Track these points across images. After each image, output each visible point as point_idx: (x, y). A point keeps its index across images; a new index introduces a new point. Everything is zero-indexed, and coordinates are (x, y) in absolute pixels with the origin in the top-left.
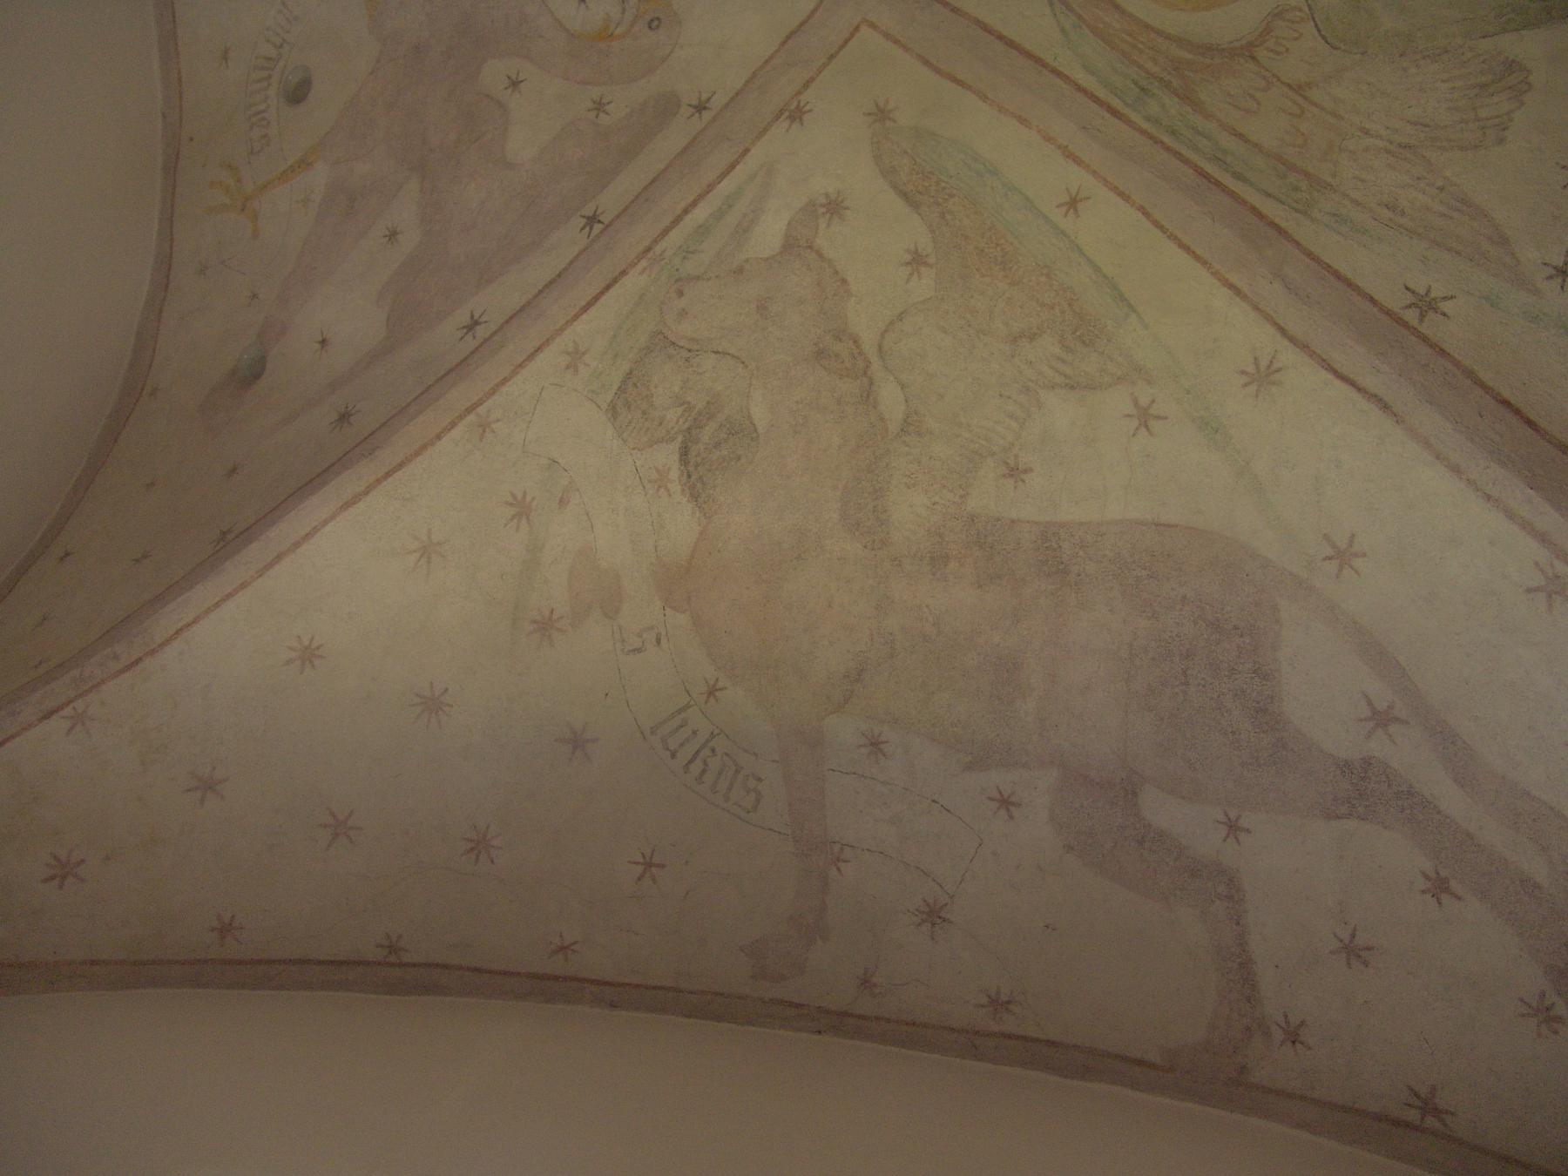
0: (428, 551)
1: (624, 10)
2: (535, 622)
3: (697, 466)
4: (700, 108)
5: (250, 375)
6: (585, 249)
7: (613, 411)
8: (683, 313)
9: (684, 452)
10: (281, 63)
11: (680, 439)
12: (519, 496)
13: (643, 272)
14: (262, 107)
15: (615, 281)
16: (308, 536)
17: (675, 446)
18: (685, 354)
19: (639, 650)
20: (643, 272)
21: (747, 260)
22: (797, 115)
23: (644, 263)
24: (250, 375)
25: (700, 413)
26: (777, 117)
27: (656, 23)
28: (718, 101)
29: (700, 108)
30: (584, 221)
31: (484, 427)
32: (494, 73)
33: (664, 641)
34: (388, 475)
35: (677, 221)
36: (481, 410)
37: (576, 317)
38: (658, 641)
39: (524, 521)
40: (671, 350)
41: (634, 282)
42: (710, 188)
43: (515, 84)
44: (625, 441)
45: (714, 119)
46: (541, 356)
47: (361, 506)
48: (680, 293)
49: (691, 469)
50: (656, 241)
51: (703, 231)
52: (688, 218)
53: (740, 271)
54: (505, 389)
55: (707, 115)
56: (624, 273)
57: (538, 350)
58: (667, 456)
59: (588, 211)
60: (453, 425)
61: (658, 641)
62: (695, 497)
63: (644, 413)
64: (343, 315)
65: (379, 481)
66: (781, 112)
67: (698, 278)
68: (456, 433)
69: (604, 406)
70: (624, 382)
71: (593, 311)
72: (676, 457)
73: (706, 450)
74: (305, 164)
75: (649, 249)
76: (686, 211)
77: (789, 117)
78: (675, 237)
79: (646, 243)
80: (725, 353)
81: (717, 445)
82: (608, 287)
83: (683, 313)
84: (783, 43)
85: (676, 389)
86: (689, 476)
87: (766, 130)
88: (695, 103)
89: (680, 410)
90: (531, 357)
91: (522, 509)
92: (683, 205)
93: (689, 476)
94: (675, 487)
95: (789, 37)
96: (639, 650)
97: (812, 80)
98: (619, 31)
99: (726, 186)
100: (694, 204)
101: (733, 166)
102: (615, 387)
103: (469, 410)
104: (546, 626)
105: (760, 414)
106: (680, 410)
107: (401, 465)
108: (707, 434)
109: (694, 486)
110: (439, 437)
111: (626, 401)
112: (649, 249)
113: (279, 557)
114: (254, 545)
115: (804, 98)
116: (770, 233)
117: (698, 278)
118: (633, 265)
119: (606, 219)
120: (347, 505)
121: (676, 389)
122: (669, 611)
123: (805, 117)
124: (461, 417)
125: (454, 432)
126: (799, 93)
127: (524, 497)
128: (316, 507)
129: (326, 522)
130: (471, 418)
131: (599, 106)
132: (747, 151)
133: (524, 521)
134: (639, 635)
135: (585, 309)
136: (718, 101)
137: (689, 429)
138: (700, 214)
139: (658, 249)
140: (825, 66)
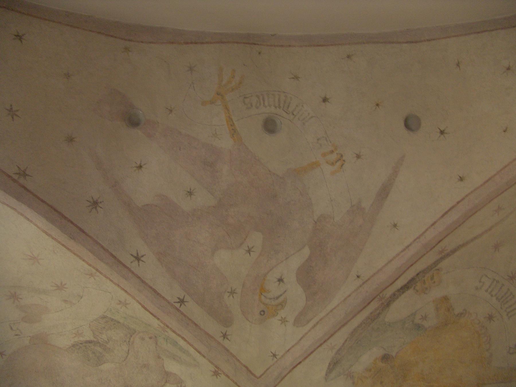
0: (34, 259)
1: (270, 299)
2: (15, 293)
3: (85, 346)
4: (225, 336)
5: (133, 122)
6: (169, 303)
7: (104, 317)
8: (143, 339)
9: (90, 342)
10: (284, 114)
11: (95, 340)
12: (65, 286)
13: (159, 325)
14: (266, 104)
15: (155, 316)
16: (28, 219)
17: (92, 338)
18: (127, 340)
19: (12, 329)
20: (159, 325)
21: (163, 359)
22: (216, 374)
23: (162, 325)
24: (133, 122)
25: (105, 346)
26: (216, 367)
27: (262, 313)
28: (226, 343)
29: (225, 336)
30: (182, 298)
31: (91, 275)
32: (256, 240)
33: (17, 337)
34: (63, 245)
35: (179, 335)
36: (98, 274)
37: (140, 304)
38: (16, 335)
39: (55, 288)
40: (129, 336)
41: (155, 323)
42: (191, 345)
43: (249, 251)
44: (92, 322)
45: (219, 343)
46: (123, 292)
47: (47, 237)
48: (151, 338)
49: (84, 344)
50: (171, 329)
51: (175, 344)
52: (180, 339)
53: (159, 357)
54: (108, 281)
55: (220, 340)
56: (158, 319)
57: (126, 291)
58: (88, 336)
59: (187, 298)
60: (90, 265)
61: (16, 335)
62: (73, 346)
63: (104, 328)
64: (155, 173)
65: (59, 242)
66: (218, 368)
67: (157, 344)
68: (86, 266)
69: (105, 314)
70: (115, 321)
71: (143, 309)
72: (88, 339)
73: (91, 349)
74: (234, 132)
75: (168, 327)
76: (183, 338)
77: (216, 371)
78: (173, 335)
79: (170, 326)
80: (128, 353)
81: (94, 353)
82: (152, 314)
83: (143, 339)
84: (244, 366)
85: (114, 338)
86: (81, 344)
87: (212, 363)
88: (227, 333)
89: (106, 340)
90: (123, 289)
91: (60, 287)
92: (185, 337)
93: (81, 344)
94: (76, 339)
95: (247, 368)
96: (12, 329)
97: (228, 377)
98: (263, 297)
99: (192, 350)
100: (185, 340)
101: (199, 352)
102: (113, 317)
103: (97, 270)
104: (14, 297)
105: (105, 367)
106: (106, 340)
107: (68, 249)
108: (99, 349)
109: (77, 345)
110: (84, 260)
111: (108, 321)
112: (168, 327)
113: (15, 209)
114: (15, 200)
115: (223, 376)
116: (172, 367)
117: (157, 344)
118: (162, 322)
119: (183, 309)
120: (46, 233)
121: (114, 338)
122: (29, 338)
123: (215, 377)
124: (94, 268)
125: (87, 265)
126: (224, 373)
127: (65, 288)
128: (42, 222)
129: (36, 225)
130: (94, 271)
131: (232, 292)
132: (204, 357)
133: (55, 288)
134: (18, 329)
135: (143, 307)
136: (226, 343)
137: (99, 343)
138: (182, 343)
139: (168, 330)
140: (233, 381)
